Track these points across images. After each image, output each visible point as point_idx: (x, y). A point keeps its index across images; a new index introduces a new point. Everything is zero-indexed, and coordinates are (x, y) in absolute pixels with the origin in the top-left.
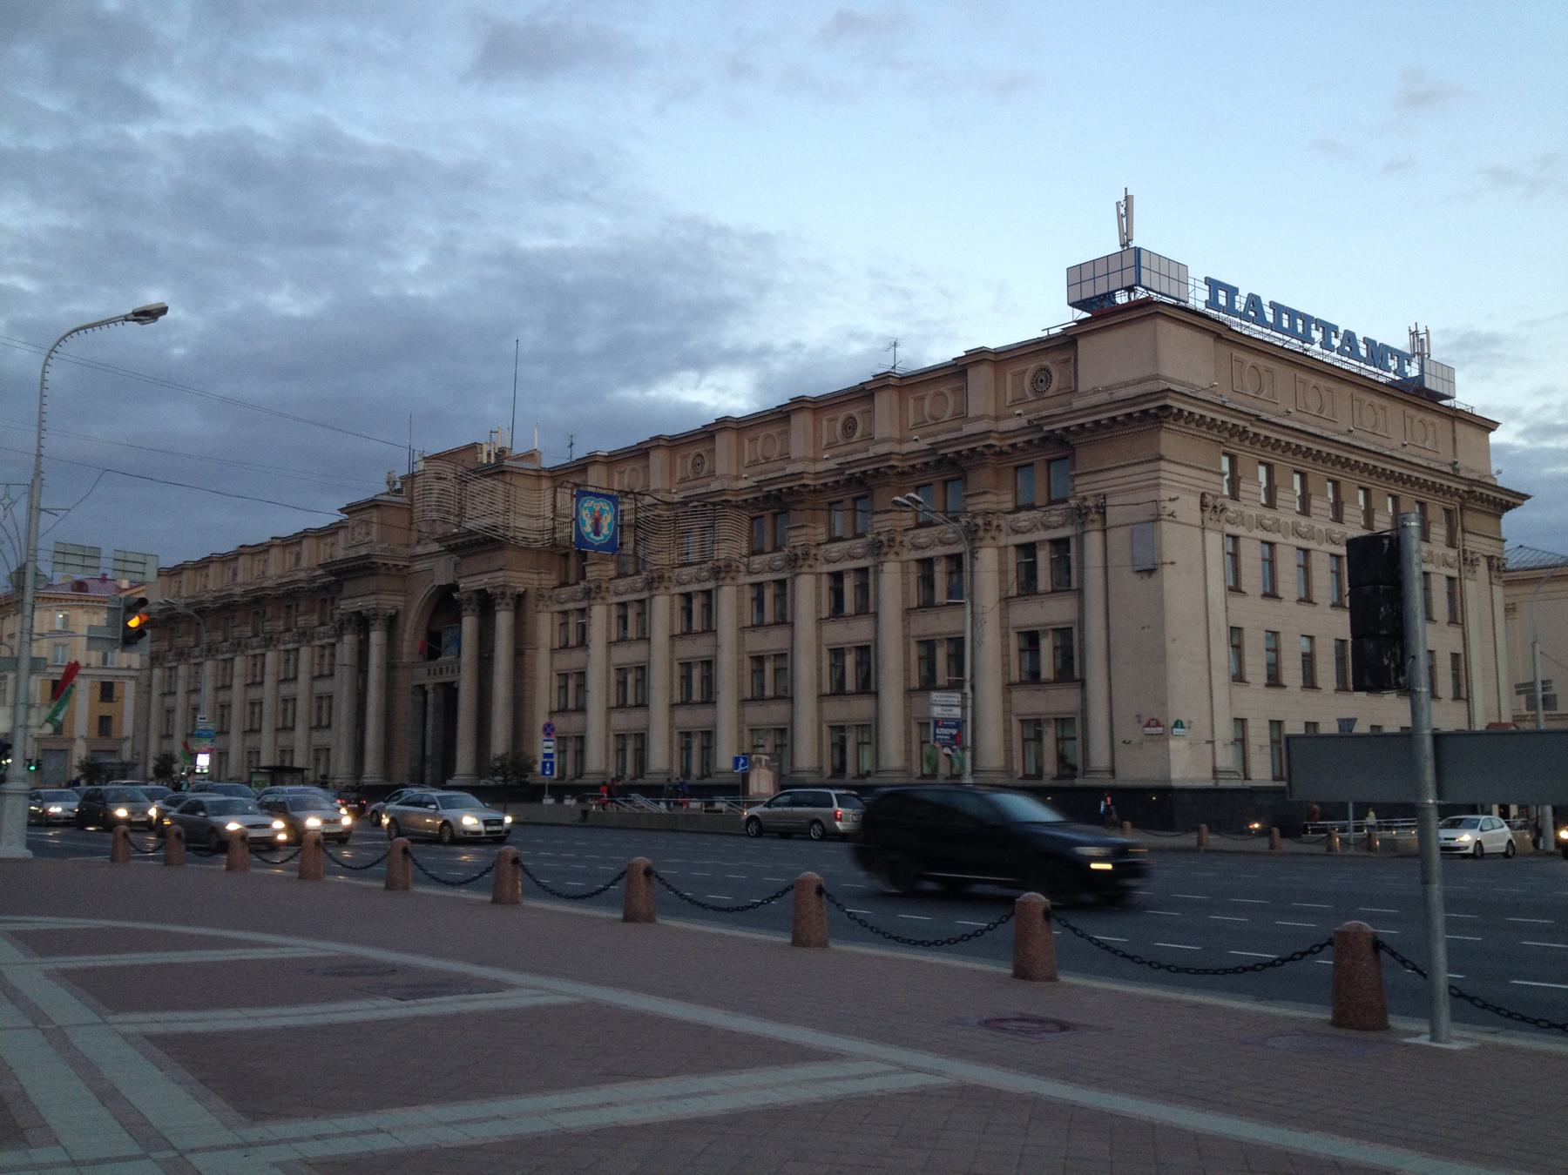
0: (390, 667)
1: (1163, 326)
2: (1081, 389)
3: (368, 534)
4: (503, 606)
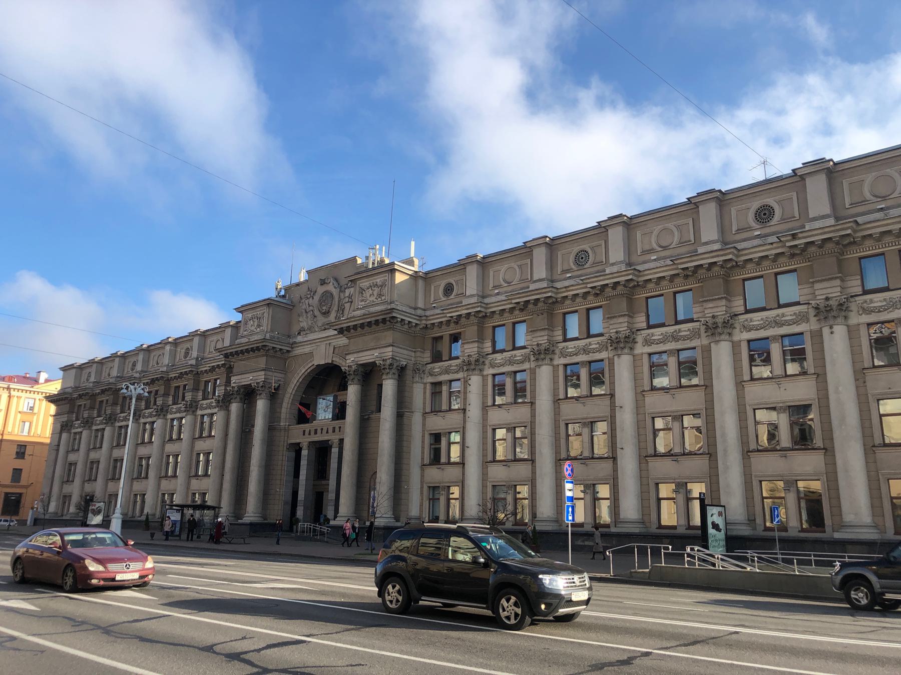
0: (271, 428)
2: (612, 261)
3: (259, 326)
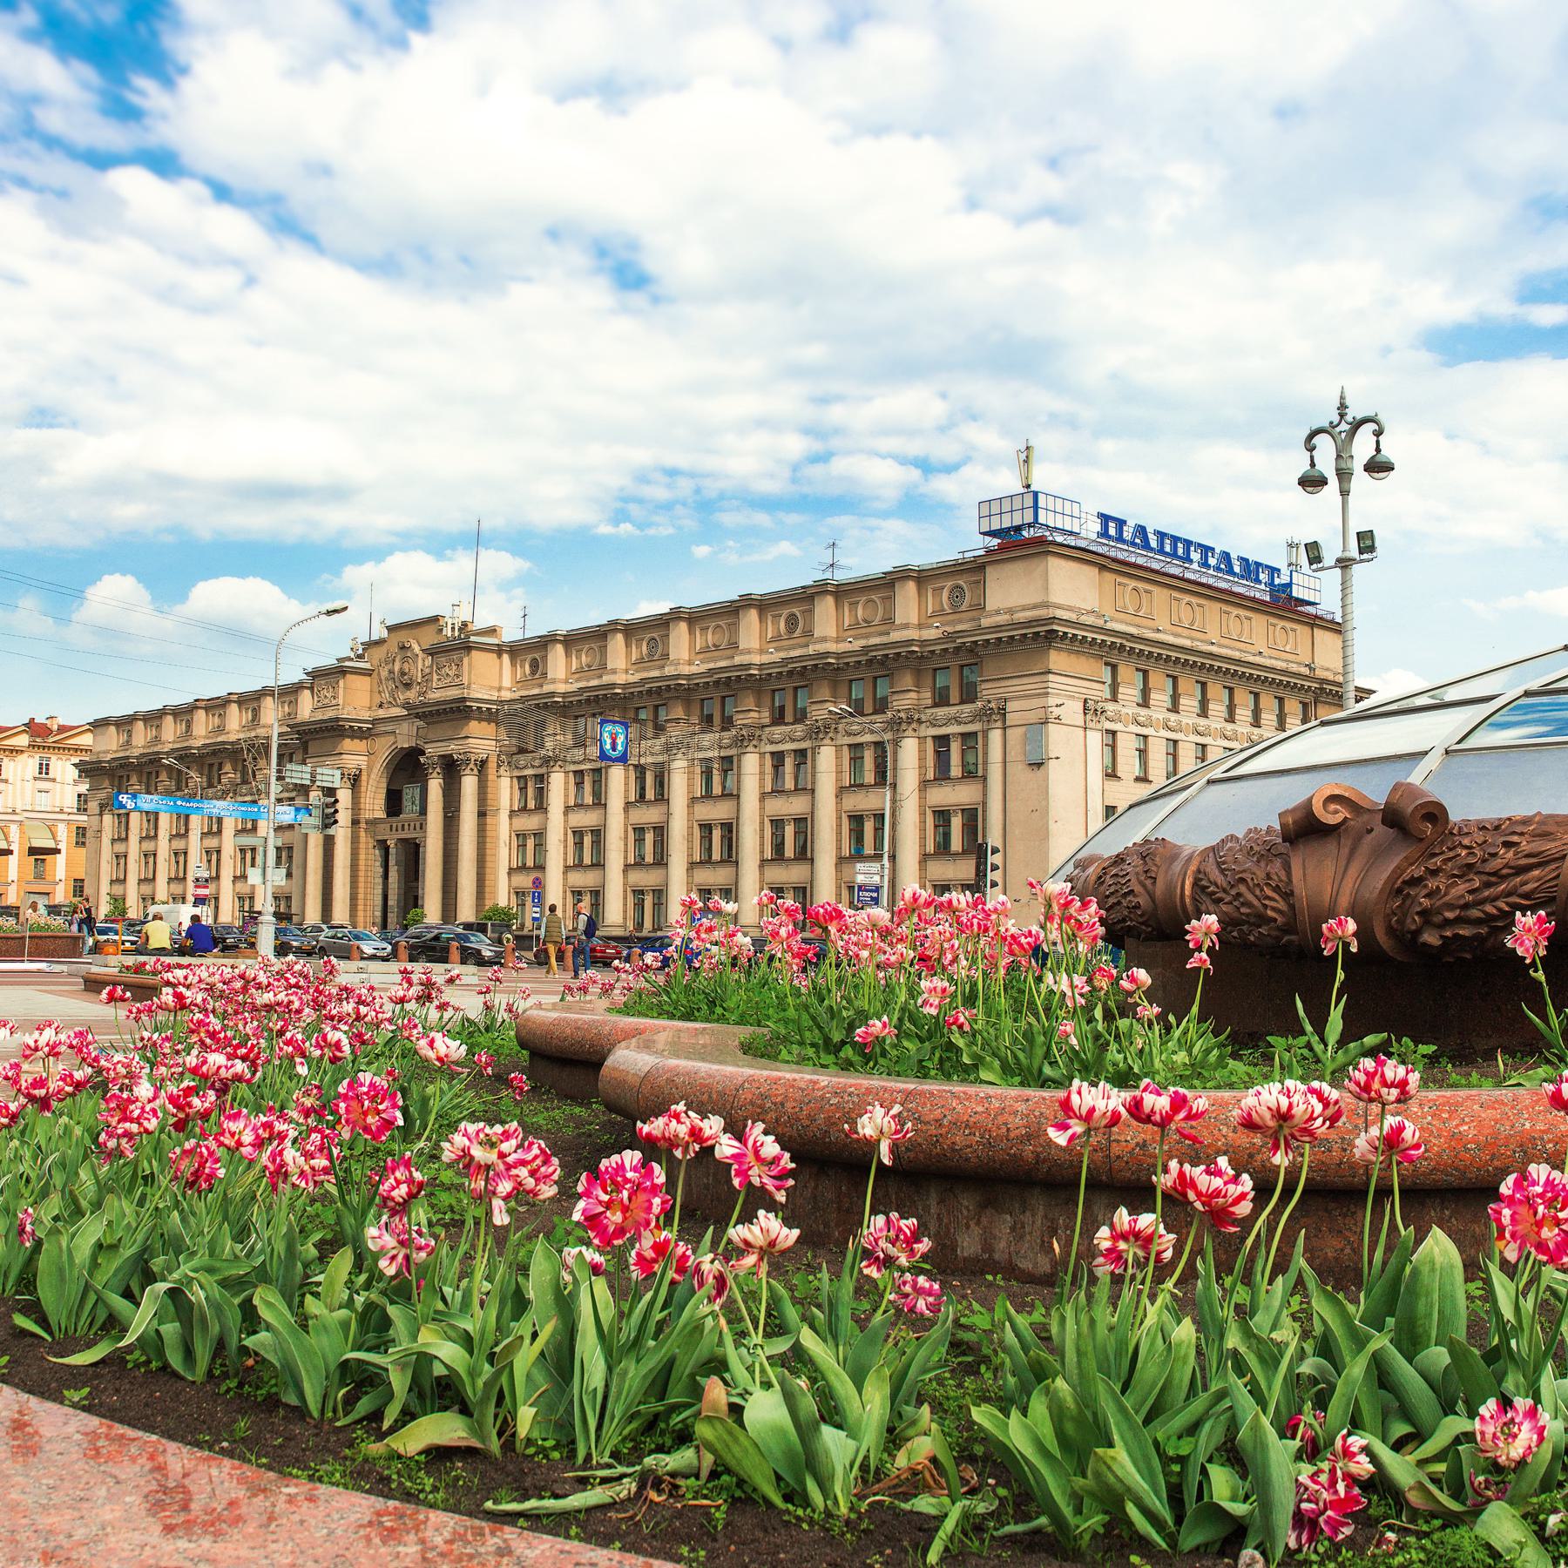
1: (1053, 562)
4: (468, 771)
